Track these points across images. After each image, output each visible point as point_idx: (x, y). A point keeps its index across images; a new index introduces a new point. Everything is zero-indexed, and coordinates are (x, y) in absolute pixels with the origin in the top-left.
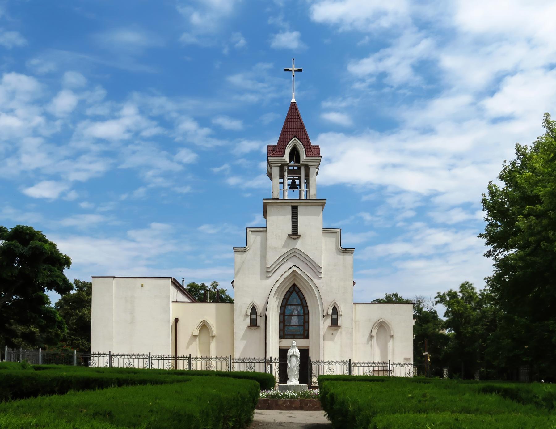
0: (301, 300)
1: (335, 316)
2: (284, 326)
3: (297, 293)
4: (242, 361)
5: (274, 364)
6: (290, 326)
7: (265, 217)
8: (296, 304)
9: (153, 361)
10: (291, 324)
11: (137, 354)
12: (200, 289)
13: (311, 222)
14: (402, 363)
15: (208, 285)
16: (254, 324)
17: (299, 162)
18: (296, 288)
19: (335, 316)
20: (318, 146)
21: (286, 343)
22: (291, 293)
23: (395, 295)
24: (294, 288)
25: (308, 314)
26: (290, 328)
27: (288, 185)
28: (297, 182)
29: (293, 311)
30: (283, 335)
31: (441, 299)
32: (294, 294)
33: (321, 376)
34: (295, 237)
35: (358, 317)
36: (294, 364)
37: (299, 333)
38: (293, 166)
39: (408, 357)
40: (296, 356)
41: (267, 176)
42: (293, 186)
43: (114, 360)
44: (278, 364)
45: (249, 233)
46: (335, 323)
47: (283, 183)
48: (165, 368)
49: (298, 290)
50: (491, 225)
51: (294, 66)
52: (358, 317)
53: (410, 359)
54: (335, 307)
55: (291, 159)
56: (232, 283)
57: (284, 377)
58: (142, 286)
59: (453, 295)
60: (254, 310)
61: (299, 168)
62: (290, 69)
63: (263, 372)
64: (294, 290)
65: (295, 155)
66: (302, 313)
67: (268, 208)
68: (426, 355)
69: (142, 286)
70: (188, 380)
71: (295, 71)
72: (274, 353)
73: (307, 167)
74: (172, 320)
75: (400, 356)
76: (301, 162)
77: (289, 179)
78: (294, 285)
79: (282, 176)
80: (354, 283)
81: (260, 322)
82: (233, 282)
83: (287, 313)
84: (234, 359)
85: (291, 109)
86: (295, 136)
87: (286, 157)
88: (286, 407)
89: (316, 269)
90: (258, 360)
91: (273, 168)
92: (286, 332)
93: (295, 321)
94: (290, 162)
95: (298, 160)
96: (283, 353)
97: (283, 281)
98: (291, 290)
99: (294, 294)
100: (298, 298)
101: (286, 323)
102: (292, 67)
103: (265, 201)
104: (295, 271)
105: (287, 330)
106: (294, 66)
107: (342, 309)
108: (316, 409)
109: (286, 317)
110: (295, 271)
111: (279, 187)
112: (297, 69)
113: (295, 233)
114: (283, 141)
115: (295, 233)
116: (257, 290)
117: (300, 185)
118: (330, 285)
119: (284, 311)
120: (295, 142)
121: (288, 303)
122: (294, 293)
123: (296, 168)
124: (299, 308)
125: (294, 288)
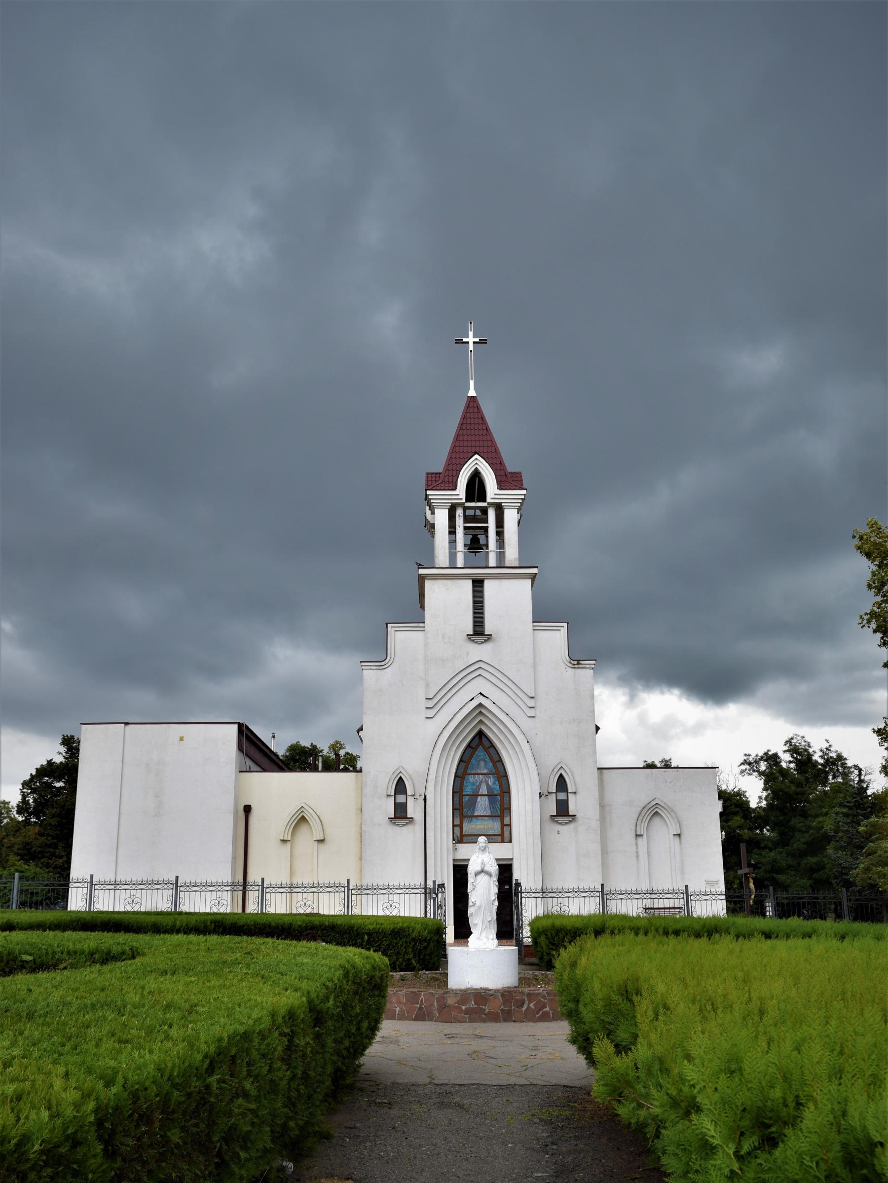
1: (562, 796)
8: (485, 771)
15: (324, 747)
16: (400, 814)
17: (485, 501)
18: (484, 739)
19: (562, 796)
20: (520, 473)
24: (480, 739)
25: (509, 792)
27: (465, 545)
28: (482, 539)
29: (479, 787)
31: (750, 764)
36: (483, 894)
40: (490, 875)
51: (471, 334)
53: (717, 882)
54: (561, 775)
58: (182, 739)
59: (772, 759)
60: (400, 787)
61: (484, 511)
62: (465, 340)
68: (746, 874)
69: (182, 739)
70: (134, 954)
71: (474, 343)
76: (489, 500)
78: (481, 734)
79: (452, 531)
81: (414, 809)
83: (468, 790)
85: (468, 407)
87: (461, 491)
88: (467, 1012)
91: (436, 511)
93: (482, 805)
94: (468, 499)
95: (482, 497)
96: (460, 872)
99: (480, 753)
100: (488, 759)
102: (468, 337)
103: (421, 571)
104: (480, 705)
106: (471, 334)
108: (545, 1018)
109: (466, 799)
110: (480, 705)
112: (477, 340)
113: (479, 631)
115: (479, 631)
116: (408, 739)
119: (462, 787)
120: (478, 463)
121: (469, 771)
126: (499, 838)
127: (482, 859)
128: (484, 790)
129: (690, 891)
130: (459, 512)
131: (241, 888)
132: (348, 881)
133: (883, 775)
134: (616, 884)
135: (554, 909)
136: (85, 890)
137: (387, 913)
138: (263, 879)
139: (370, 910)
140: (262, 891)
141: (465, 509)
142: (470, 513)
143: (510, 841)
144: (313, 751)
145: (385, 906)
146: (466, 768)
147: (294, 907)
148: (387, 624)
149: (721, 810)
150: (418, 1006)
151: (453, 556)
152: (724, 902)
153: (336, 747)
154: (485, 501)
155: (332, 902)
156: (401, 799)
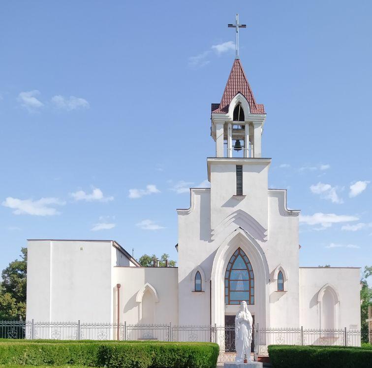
0: (246, 264)
1: (281, 281)
3: (242, 257)
5: (218, 332)
7: (209, 180)
15: (159, 257)
16: (198, 290)
17: (244, 121)
19: (281, 281)
21: (233, 310)
22: (236, 257)
24: (239, 251)
27: (233, 146)
30: (229, 301)
34: (239, 197)
35: (303, 283)
38: (237, 125)
39: (354, 323)
42: (237, 147)
43: (349, 337)
44: (223, 332)
45: (193, 193)
46: (281, 288)
47: (227, 144)
49: (243, 255)
50: (234, 328)
52: (303, 283)
53: (356, 326)
54: (280, 271)
55: (235, 118)
58: (81, 249)
61: (243, 127)
63: (208, 341)
64: (239, 254)
65: (239, 114)
66: (248, 278)
67: (212, 167)
69: (81, 249)
72: (219, 321)
73: (251, 124)
74: (114, 285)
78: (239, 249)
79: (226, 138)
80: (300, 246)
81: (204, 287)
86: (239, 92)
89: (260, 231)
90: (202, 328)
93: (240, 286)
94: (234, 120)
95: (242, 119)
96: (230, 320)
97: (228, 279)
98: (236, 254)
103: (209, 160)
105: (233, 296)
107: (288, 274)
111: (223, 147)
114: (227, 97)
117: (244, 147)
118: (275, 249)
122: (239, 256)
124: (245, 273)
127: (245, 314)
130: (230, 126)
131: (117, 327)
137: (191, 340)
138: (33, 320)
139: (85, 336)
140: (79, 327)
141: (233, 125)
142: (235, 127)
144: (155, 260)
147: (286, 337)
149: (361, 290)
153: (165, 257)
154: (244, 121)
156: (198, 282)
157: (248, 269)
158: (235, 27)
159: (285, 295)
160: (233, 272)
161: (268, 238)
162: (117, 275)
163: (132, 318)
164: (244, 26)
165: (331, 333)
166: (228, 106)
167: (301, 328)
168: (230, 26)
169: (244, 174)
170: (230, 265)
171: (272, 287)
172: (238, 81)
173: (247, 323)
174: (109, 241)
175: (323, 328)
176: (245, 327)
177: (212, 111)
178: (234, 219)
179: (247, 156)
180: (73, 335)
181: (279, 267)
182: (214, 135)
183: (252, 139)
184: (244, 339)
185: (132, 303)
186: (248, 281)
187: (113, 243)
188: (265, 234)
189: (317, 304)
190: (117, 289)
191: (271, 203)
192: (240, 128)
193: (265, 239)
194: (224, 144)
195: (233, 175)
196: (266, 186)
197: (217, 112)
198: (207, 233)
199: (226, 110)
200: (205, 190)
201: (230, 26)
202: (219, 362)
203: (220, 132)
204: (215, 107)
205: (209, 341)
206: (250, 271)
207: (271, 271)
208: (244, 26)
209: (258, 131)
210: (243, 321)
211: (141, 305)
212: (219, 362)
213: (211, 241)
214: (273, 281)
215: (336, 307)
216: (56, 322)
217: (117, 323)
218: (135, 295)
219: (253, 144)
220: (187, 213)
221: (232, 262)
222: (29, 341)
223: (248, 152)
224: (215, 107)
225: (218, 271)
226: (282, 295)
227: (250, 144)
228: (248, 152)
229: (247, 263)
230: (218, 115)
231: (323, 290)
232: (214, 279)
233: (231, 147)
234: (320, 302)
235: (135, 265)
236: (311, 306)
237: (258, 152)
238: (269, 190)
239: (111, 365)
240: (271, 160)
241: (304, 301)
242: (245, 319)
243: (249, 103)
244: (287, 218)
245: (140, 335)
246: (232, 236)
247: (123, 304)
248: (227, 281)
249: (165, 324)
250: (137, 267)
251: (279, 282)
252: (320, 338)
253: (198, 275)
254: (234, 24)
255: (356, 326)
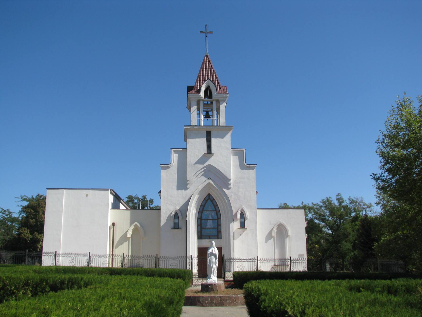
1: (242, 220)
2: (201, 228)
4: (65, 255)
6: (205, 228)
8: (211, 210)
9: (260, 263)
10: (207, 227)
11: (79, 253)
12: (135, 199)
13: (221, 145)
14: (296, 258)
16: (176, 227)
18: (210, 197)
19: (242, 220)
21: (205, 243)
22: (207, 201)
23: (285, 204)
24: (209, 197)
26: (206, 230)
28: (210, 113)
30: (200, 236)
32: (209, 202)
33: (236, 272)
34: (209, 155)
35: (262, 221)
37: (213, 235)
38: (208, 100)
39: (302, 253)
41: (187, 109)
42: (207, 116)
44: (196, 261)
45: (173, 152)
46: (242, 226)
48: (170, 268)
49: (212, 199)
56: (159, 193)
57: (203, 273)
58: (87, 196)
61: (212, 103)
64: (209, 198)
65: (208, 93)
66: (216, 217)
69: (87, 196)
72: (193, 251)
73: (218, 102)
74: (110, 224)
75: (297, 254)
76: (213, 98)
77: (204, 111)
78: (209, 194)
81: (181, 224)
82: (160, 192)
83: (204, 217)
84: (59, 254)
86: (208, 79)
92: (203, 234)
93: (210, 224)
95: (211, 97)
96: (203, 253)
98: (206, 199)
99: (209, 202)
100: (212, 205)
101: (203, 226)
105: (205, 232)
107: (248, 214)
109: (203, 221)
111: (196, 118)
114: (200, 81)
117: (212, 116)
121: (205, 209)
122: (209, 200)
123: (209, 103)
124: (214, 214)
125: (209, 197)
126: (216, 237)
128: (210, 217)
129: (57, 253)
132: (89, 253)
133: (150, 199)
134: (163, 254)
135: (137, 264)
136: (53, 257)
141: (203, 101)
143: (221, 239)
145: (103, 263)
146: (203, 209)
148: (171, 149)
150: (190, 301)
151: (199, 121)
152: (307, 263)
155: (301, 265)
156: (176, 221)
157: (216, 210)
158: (205, 33)
159: (246, 231)
160: (205, 213)
161: (232, 186)
162: (112, 216)
163: (124, 249)
164: (211, 32)
165: (283, 261)
166: (200, 88)
167: (289, 258)
168: (201, 32)
169: (213, 141)
170: (202, 207)
171: (235, 226)
172: (207, 70)
173: (215, 255)
174: (107, 189)
175: (277, 257)
176: (213, 257)
177: (188, 92)
178: (203, 173)
179: (214, 124)
180: (184, 256)
181: (241, 208)
182: (189, 108)
183: (218, 110)
184: (213, 265)
185: (124, 238)
186: (216, 220)
187: (110, 191)
188: (229, 183)
189: (272, 238)
190: (112, 226)
191: (234, 160)
192: (209, 103)
193: (229, 187)
194: (197, 114)
195: (204, 141)
196: (230, 147)
197: (190, 93)
198: (182, 183)
199: (199, 91)
200: (181, 149)
201: (201, 32)
202: (184, 260)
203: (194, 108)
204: (190, 89)
205: (185, 268)
206: (217, 212)
207: (234, 213)
208: (211, 32)
209: (223, 107)
210: (212, 254)
211: (130, 239)
212: (184, 260)
213: (186, 189)
214: (237, 220)
215: (287, 240)
216: (241, 258)
217: (111, 254)
218: (126, 233)
219: (219, 114)
220: (168, 168)
221: (200, 218)
222: (50, 270)
223: (215, 120)
224: (190, 89)
225: (193, 212)
226: (244, 232)
227: (216, 114)
228: (215, 120)
229: (216, 206)
230: (192, 95)
231: (276, 228)
232: (189, 219)
233: (202, 117)
234: (274, 237)
235: (126, 207)
236: (266, 241)
237: (223, 121)
238: (231, 150)
239: (396, 163)
240: (233, 127)
241: (261, 236)
242: (214, 252)
243: (216, 86)
244: (246, 171)
245: (130, 264)
246: (203, 185)
247: (117, 239)
248: (199, 220)
249: (253, 258)
250: (127, 209)
251: (241, 221)
252: (275, 265)
253: (176, 216)
254: (204, 31)
255: (302, 255)
